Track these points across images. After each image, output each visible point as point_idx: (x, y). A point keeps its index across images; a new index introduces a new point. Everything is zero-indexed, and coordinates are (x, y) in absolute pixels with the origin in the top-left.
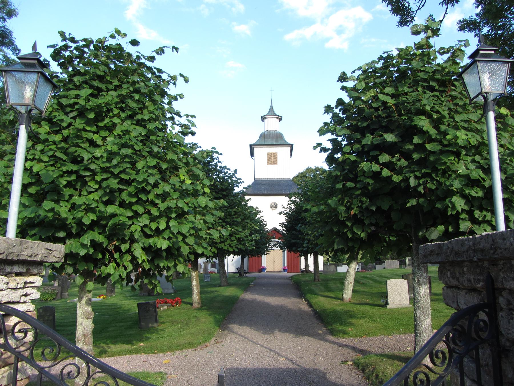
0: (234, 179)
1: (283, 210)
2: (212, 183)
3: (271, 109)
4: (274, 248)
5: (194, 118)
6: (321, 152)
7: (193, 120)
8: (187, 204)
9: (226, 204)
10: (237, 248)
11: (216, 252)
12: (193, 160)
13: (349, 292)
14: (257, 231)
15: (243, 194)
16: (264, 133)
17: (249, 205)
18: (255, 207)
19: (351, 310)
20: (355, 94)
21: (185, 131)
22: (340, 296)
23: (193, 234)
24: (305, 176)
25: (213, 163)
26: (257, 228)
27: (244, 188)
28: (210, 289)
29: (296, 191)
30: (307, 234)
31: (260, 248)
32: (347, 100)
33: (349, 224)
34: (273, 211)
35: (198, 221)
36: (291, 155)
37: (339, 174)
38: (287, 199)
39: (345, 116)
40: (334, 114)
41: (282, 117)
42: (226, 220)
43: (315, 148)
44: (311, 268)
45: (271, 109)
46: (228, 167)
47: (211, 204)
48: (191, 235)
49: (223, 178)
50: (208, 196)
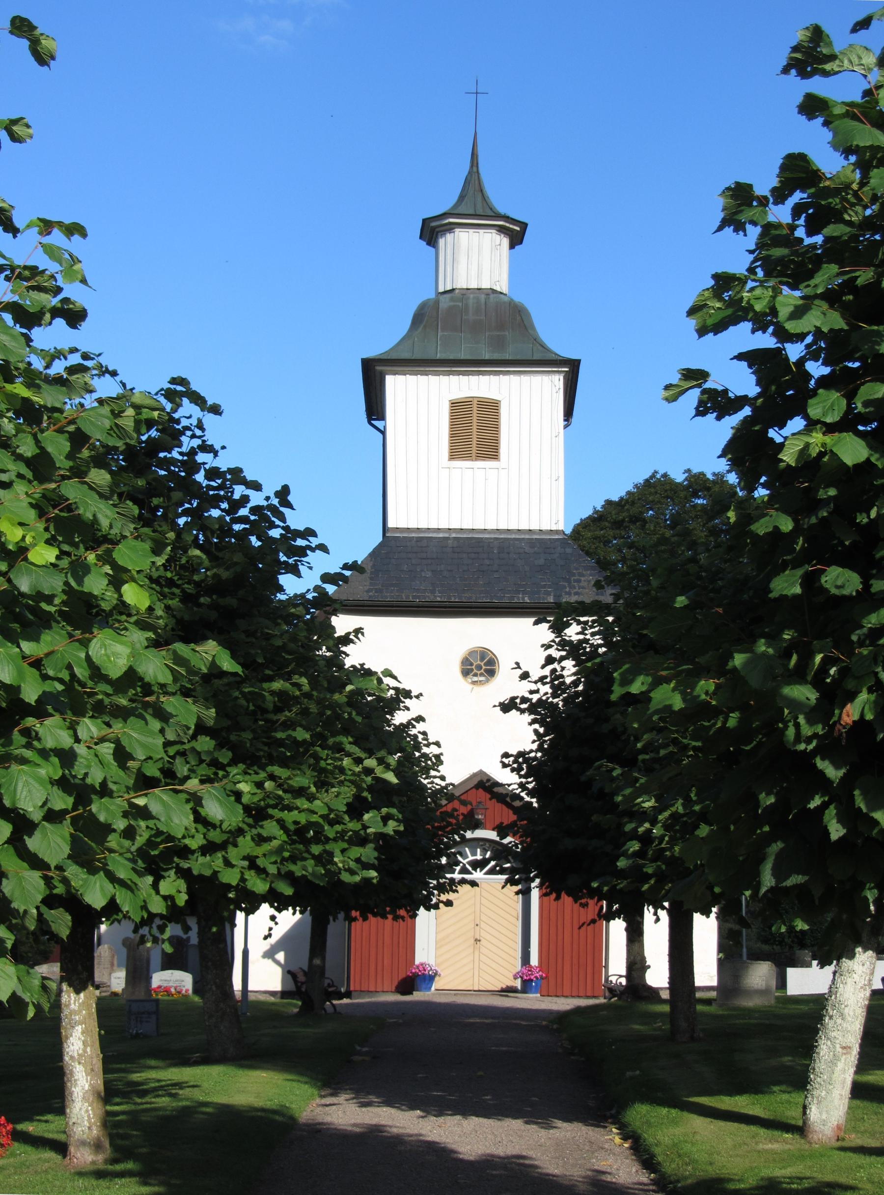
0: (275, 533)
1: (522, 689)
3: (473, 184)
4: (478, 875)
5: (76, 238)
6: (701, 411)
7: (75, 245)
8: (37, 664)
9: (228, 664)
10: (290, 877)
11: (182, 899)
12: (67, 446)
13: (836, 1093)
14: (382, 793)
15: (326, 605)
16: (437, 302)
17: (348, 663)
19: (843, 1179)
20: (868, 136)
21: (34, 300)
22: (792, 1115)
23: (64, 812)
24: (638, 519)
25: (175, 454)
26: (391, 777)
27: (327, 578)
28: (153, 1074)
29: (589, 595)
30: (642, 816)
31: (409, 877)
32: (831, 163)
33: (833, 773)
34: (468, 698)
35: (90, 742)
36: (568, 413)
37: (786, 525)
38: (544, 633)
39: (818, 239)
40: (768, 227)
41: (524, 226)
43: (673, 393)
44: (658, 975)
45: (473, 184)
46: (250, 476)
47: (155, 668)
48: (53, 816)
49: (224, 530)
50: (143, 625)
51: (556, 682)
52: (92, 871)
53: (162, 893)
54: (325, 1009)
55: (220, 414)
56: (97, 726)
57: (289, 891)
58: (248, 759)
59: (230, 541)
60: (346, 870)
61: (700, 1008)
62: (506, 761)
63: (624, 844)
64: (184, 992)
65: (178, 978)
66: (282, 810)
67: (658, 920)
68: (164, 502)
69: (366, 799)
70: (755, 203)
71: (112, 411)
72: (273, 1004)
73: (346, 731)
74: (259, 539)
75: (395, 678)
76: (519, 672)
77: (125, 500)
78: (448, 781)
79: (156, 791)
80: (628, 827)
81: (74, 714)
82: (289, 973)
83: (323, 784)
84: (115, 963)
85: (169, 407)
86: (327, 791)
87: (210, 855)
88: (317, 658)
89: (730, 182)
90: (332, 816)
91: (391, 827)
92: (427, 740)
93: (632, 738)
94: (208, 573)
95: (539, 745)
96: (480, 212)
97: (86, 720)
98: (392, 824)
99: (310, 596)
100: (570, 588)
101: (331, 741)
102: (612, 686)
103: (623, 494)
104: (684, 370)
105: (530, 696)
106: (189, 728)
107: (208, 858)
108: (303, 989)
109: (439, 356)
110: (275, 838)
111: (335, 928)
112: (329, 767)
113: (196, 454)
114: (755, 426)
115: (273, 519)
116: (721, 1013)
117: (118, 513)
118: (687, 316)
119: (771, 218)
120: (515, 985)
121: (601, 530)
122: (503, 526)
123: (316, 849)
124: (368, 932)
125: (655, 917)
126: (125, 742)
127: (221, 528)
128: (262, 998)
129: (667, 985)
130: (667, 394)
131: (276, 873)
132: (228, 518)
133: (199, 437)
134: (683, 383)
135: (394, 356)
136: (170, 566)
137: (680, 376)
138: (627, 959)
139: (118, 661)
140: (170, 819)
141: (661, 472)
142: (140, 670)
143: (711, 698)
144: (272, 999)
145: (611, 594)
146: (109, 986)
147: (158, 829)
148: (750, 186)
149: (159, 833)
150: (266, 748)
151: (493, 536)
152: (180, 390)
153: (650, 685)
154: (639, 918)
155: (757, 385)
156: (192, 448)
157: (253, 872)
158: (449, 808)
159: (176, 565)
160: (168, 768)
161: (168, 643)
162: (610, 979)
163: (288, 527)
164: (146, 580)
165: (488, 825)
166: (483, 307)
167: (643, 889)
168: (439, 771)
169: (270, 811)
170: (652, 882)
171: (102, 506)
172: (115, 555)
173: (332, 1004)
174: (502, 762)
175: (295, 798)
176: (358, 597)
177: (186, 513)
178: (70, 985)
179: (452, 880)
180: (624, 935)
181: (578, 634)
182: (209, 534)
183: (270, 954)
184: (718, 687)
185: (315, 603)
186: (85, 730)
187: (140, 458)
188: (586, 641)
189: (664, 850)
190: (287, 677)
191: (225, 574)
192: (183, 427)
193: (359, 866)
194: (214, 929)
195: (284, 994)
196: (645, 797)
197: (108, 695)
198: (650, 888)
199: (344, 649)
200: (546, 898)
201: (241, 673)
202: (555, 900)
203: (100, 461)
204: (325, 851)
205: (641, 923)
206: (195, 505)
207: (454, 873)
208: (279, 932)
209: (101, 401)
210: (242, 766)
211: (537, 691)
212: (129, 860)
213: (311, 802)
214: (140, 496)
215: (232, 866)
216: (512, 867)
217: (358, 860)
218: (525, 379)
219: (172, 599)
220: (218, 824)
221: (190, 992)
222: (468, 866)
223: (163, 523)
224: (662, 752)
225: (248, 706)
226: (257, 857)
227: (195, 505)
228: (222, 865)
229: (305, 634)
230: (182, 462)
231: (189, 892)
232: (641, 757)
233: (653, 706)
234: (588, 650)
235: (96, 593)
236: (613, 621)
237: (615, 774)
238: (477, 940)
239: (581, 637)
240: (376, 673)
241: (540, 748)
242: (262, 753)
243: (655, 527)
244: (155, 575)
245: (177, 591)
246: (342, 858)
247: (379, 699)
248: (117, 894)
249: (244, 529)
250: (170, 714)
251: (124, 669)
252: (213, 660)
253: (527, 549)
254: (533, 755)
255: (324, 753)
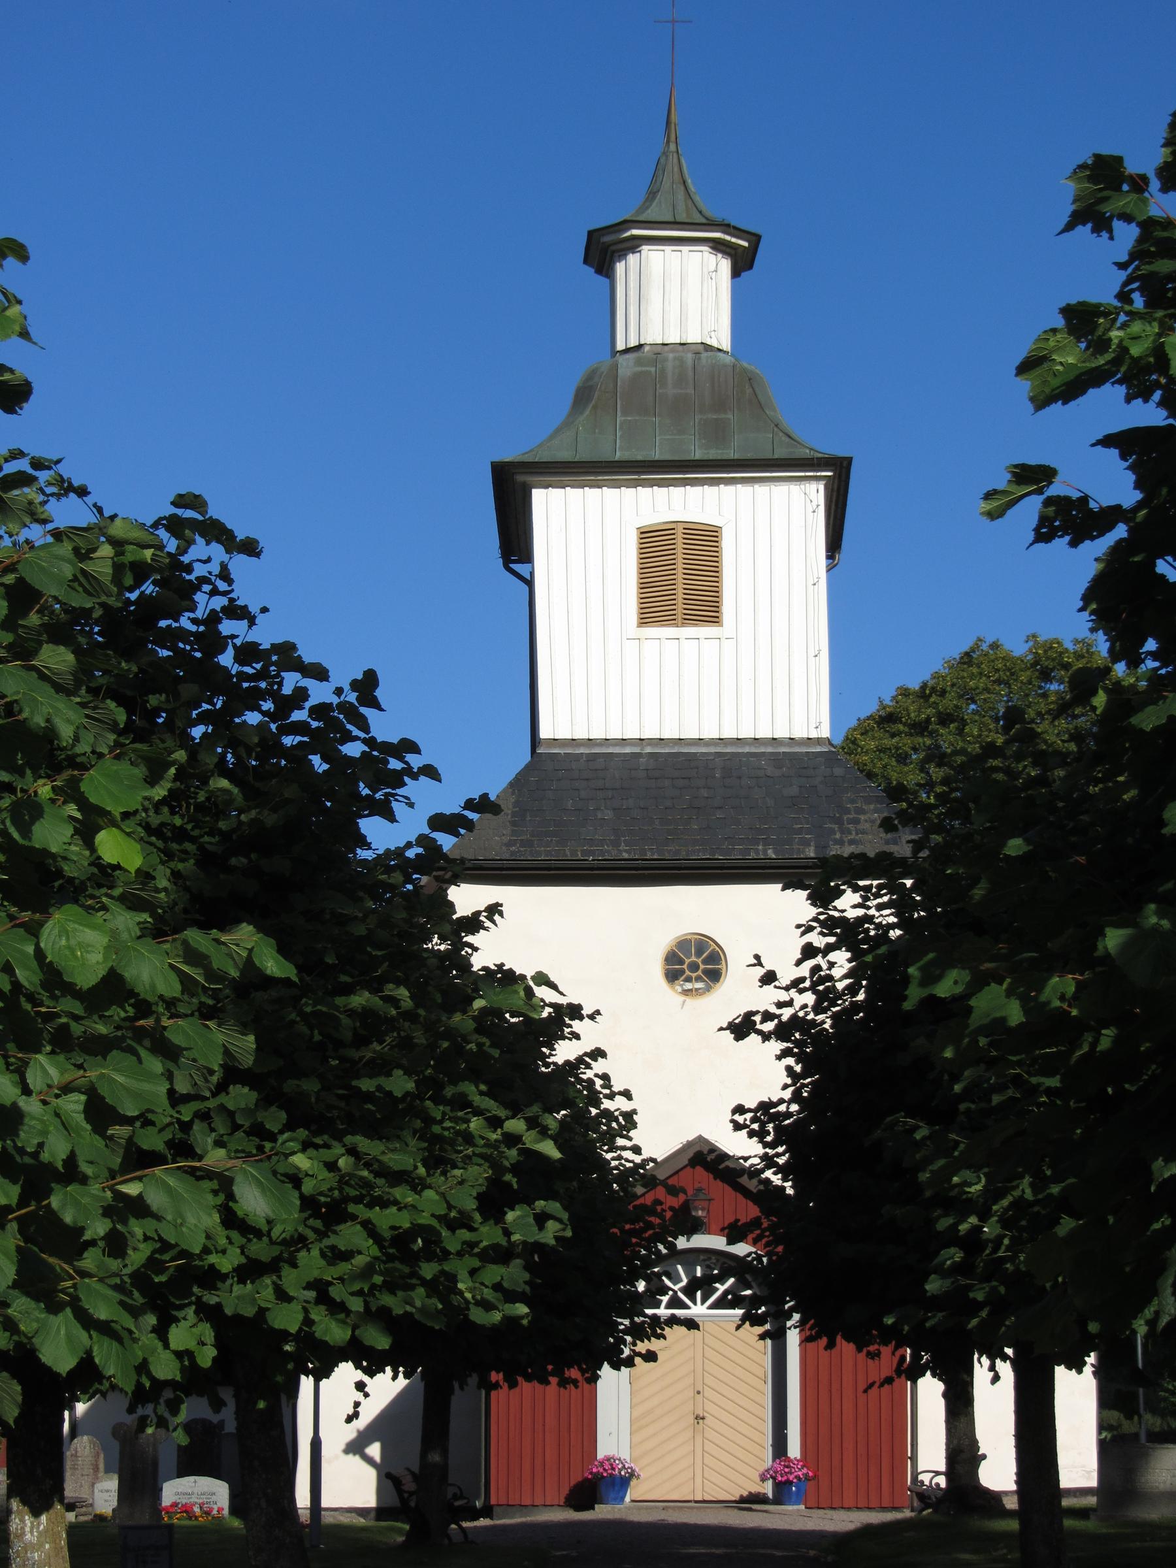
0: (353, 750)
1: (766, 999)
2: (159, 792)
4: (698, 1310)
6: (1044, 534)
9: (273, 965)
10: (383, 1317)
11: (207, 1356)
14: (535, 1178)
17: (478, 962)
18: (529, 974)
25: (185, 622)
26: (550, 1149)
27: (439, 822)
29: (873, 843)
30: (961, 1205)
31: (585, 1311)
34: (676, 1019)
36: (834, 544)
38: (796, 905)
42: (290, 1085)
43: (999, 505)
44: (999, 1472)
46: (308, 656)
47: (153, 971)
49: (269, 745)
50: (132, 903)
51: (821, 988)
52: (54, 1308)
53: (173, 1346)
54: (449, 1537)
55: (257, 555)
56: (57, 1065)
57: (382, 1342)
58: (315, 1124)
59: (278, 763)
60: (478, 1303)
61: (1068, 1523)
62: (740, 1119)
63: (937, 1253)
64: (215, 1512)
65: (206, 1489)
66: (370, 1206)
67: (996, 1378)
68: (168, 701)
69: (509, 1184)
70: (1125, 187)
71: (76, 550)
72: (363, 1529)
73: (475, 1075)
74: (325, 759)
75: (554, 987)
76: (760, 972)
77: (104, 699)
78: (646, 1154)
79: (158, 1171)
80: (943, 1224)
81: (21, 1048)
82: (388, 1477)
83: (438, 1161)
84: (102, 1466)
85: (172, 545)
86: (444, 1173)
87: (252, 1283)
88: (425, 955)
89: (1086, 157)
90: (453, 1214)
91: (550, 1233)
92: (609, 1087)
93: (946, 1077)
94: (243, 817)
95: (794, 1093)
96: (682, 217)
97: (40, 1057)
98: (551, 1225)
99: (411, 854)
100: (842, 832)
101: (449, 1091)
102: (906, 988)
103: (926, 677)
104: (1016, 466)
105: (778, 1012)
106: (211, 1072)
107: (249, 1286)
108: (413, 1504)
109: (618, 456)
110: (360, 1253)
111: (460, 1401)
112: (446, 1133)
113: (219, 621)
114: (1134, 555)
115: (349, 727)
116: (1104, 1531)
117: (87, 716)
118: (1017, 375)
119: (1154, 211)
120: (763, 1491)
121: (893, 736)
122: (729, 733)
123: (428, 1270)
124: (516, 1408)
125: (992, 1373)
126: (103, 1091)
127: (263, 741)
128: (345, 1519)
129: (1014, 1487)
130: (989, 507)
131: (362, 1310)
132: (273, 727)
133: (225, 593)
134: (1013, 488)
135: (545, 456)
136: (180, 807)
137: (1009, 476)
138: (948, 1444)
139: (89, 956)
140: (181, 1216)
141: (990, 639)
142: (128, 974)
143: (1070, 1006)
144: (362, 1521)
145: (908, 842)
146: (92, 1505)
147: (161, 1240)
148: (1119, 160)
149: (165, 1246)
150: (342, 1104)
151: (712, 750)
152: (192, 519)
153: (969, 985)
154: (965, 1376)
155: (1135, 488)
156: (213, 611)
157: (322, 1308)
158: (648, 1200)
159: (188, 805)
160: (180, 1140)
161: (176, 930)
162: (920, 1477)
163: (373, 738)
164: (140, 829)
165: (713, 1227)
166: (690, 373)
167: (970, 1326)
168: (630, 1139)
169: (352, 1208)
170: (984, 1314)
171: (61, 706)
172: (84, 787)
173: (460, 1527)
174: (732, 1121)
175: (392, 1186)
176: (492, 855)
177: (203, 718)
178: (24, 1502)
179: (655, 1318)
180: (941, 1404)
181: (854, 907)
182: (242, 751)
183: (356, 1447)
184: (1080, 986)
185: (421, 864)
186: (39, 1073)
187: (129, 628)
188: (869, 919)
189: (1002, 1260)
190: (376, 987)
191: (271, 819)
192: (197, 578)
193: (499, 1295)
194: (261, 1405)
195: (381, 1512)
196: (968, 1174)
197: (76, 1018)
198: (979, 1324)
199: (469, 939)
200: (810, 1345)
201: (295, 979)
202: (826, 1348)
203: (58, 633)
204: (443, 1272)
205: (970, 1384)
206: (219, 706)
207: (658, 1307)
208: (371, 1410)
209: (57, 535)
210: (302, 1133)
211: (789, 1003)
212: (116, 1288)
213: (419, 1193)
214: (129, 693)
215: (288, 1299)
216: (754, 1295)
217: (497, 1287)
218: (761, 490)
219: (182, 861)
220: (265, 1228)
221: (226, 1512)
222: (680, 1295)
223: (167, 736)
224: (996, 1099)
225: (312, 1036)
226: (330, 1284)
227: (219, 705)
228: (272, 1297)
229: (404, 915)
230: (196, 634)
231: (218, 1344)
232: (963, 1107)
233: (975, 1021)
234: (872, 933)
235: (54, 850)
236: (913, 885)
237: (918, 1136)
238: (699, 1418)
239: (860, 912)
240: (523, 977)
241: (796, 1097)
242: (335, 1113)
243: (980, 730)
244: (155, 820)
245: (190, 847)
246: (470, 1284)
247: (528, 1021)
248: (95, 1348)
249: (300, 742)
250: (179, 1047)
251: (102, 972)
252: (250, 956)
253: (770, 771)
254: (782, 1108)
255: (437, 1112)
